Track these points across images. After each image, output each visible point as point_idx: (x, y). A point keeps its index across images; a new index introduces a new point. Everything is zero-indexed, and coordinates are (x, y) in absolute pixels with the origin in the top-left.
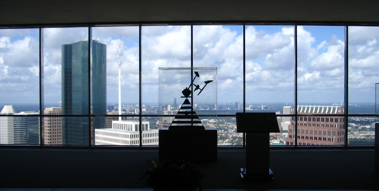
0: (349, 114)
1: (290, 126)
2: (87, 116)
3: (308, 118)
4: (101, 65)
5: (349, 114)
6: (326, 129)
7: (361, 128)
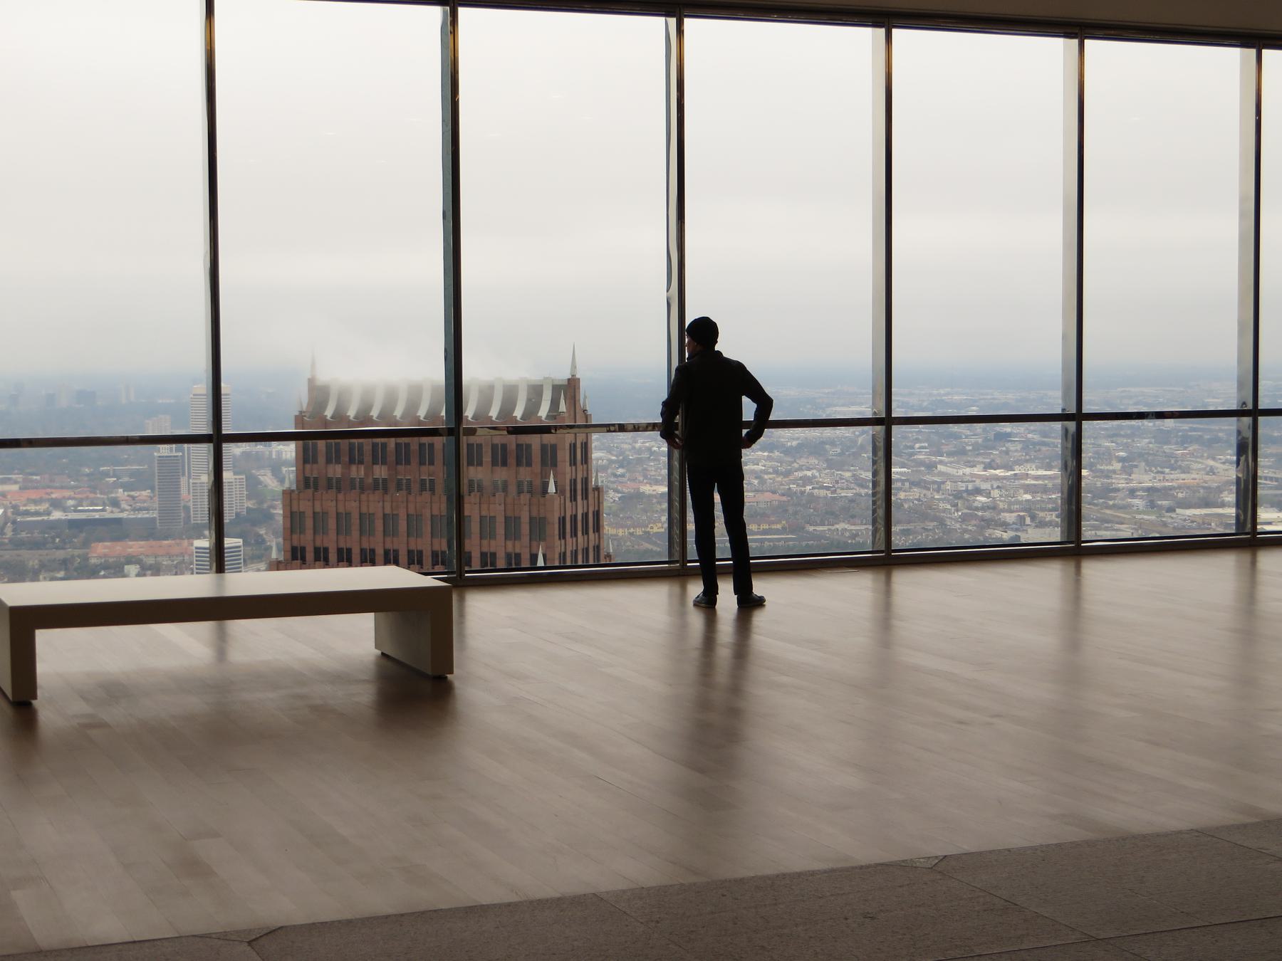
0: (226, 430)
1: (295, 496)
2: (1248, 449)
3: (370, 447)
4: (214, 936)
5: (226, 430)
6: (375, 505)
7: (620, 498)
